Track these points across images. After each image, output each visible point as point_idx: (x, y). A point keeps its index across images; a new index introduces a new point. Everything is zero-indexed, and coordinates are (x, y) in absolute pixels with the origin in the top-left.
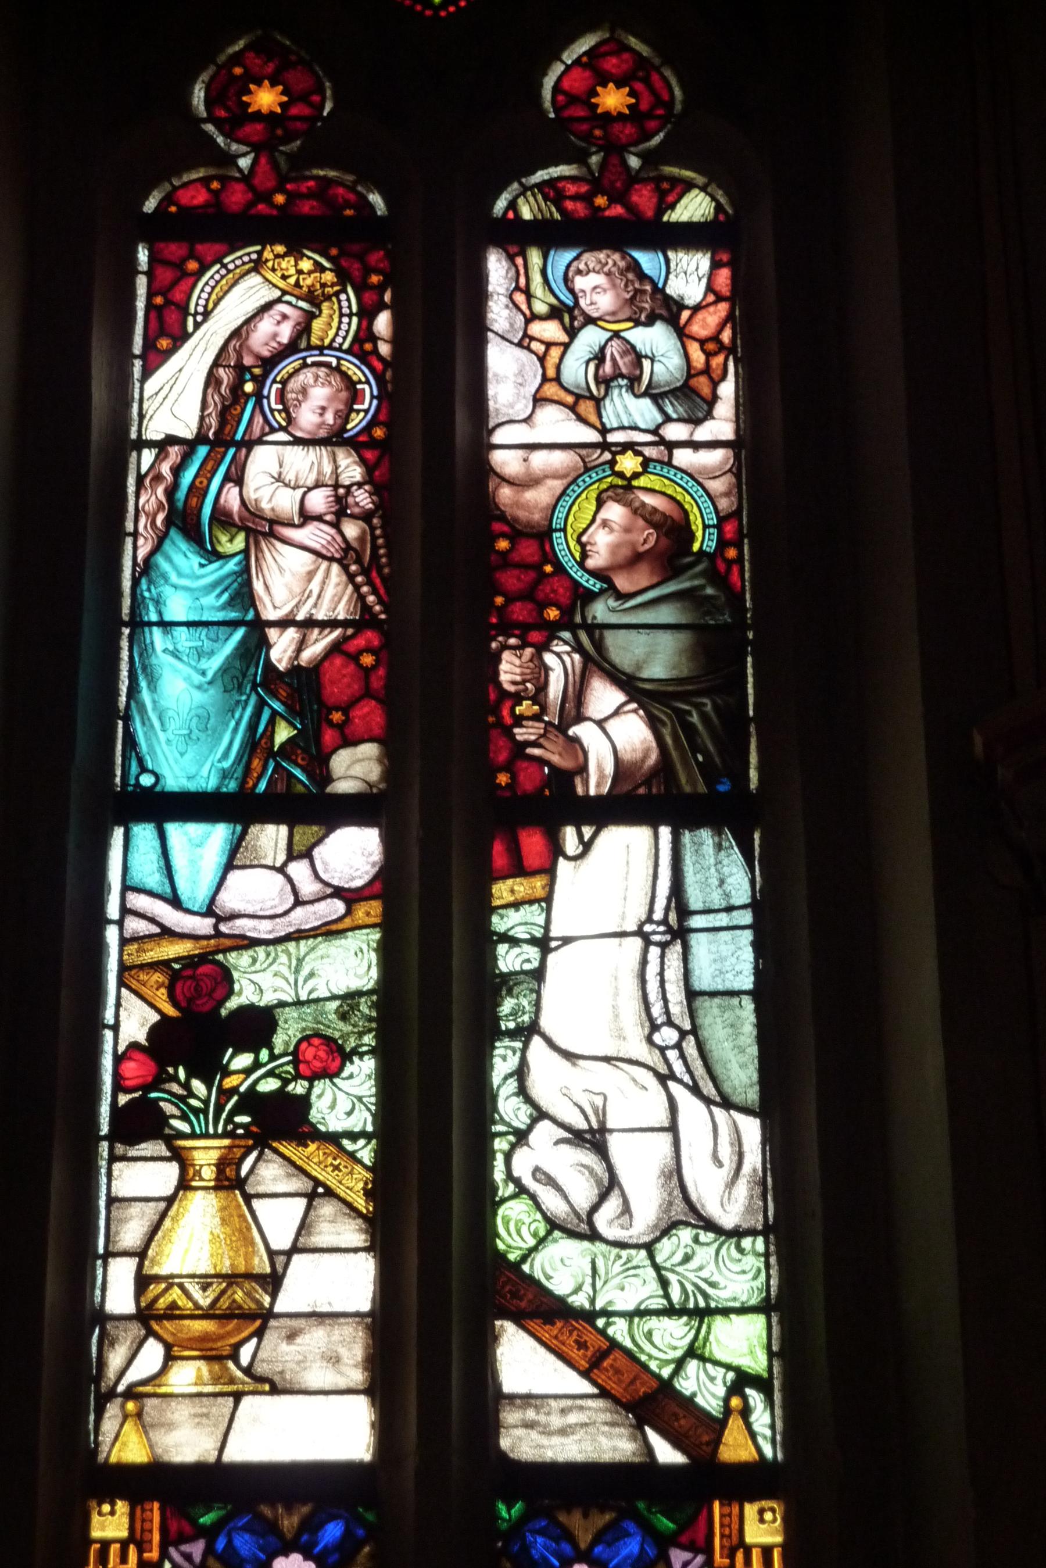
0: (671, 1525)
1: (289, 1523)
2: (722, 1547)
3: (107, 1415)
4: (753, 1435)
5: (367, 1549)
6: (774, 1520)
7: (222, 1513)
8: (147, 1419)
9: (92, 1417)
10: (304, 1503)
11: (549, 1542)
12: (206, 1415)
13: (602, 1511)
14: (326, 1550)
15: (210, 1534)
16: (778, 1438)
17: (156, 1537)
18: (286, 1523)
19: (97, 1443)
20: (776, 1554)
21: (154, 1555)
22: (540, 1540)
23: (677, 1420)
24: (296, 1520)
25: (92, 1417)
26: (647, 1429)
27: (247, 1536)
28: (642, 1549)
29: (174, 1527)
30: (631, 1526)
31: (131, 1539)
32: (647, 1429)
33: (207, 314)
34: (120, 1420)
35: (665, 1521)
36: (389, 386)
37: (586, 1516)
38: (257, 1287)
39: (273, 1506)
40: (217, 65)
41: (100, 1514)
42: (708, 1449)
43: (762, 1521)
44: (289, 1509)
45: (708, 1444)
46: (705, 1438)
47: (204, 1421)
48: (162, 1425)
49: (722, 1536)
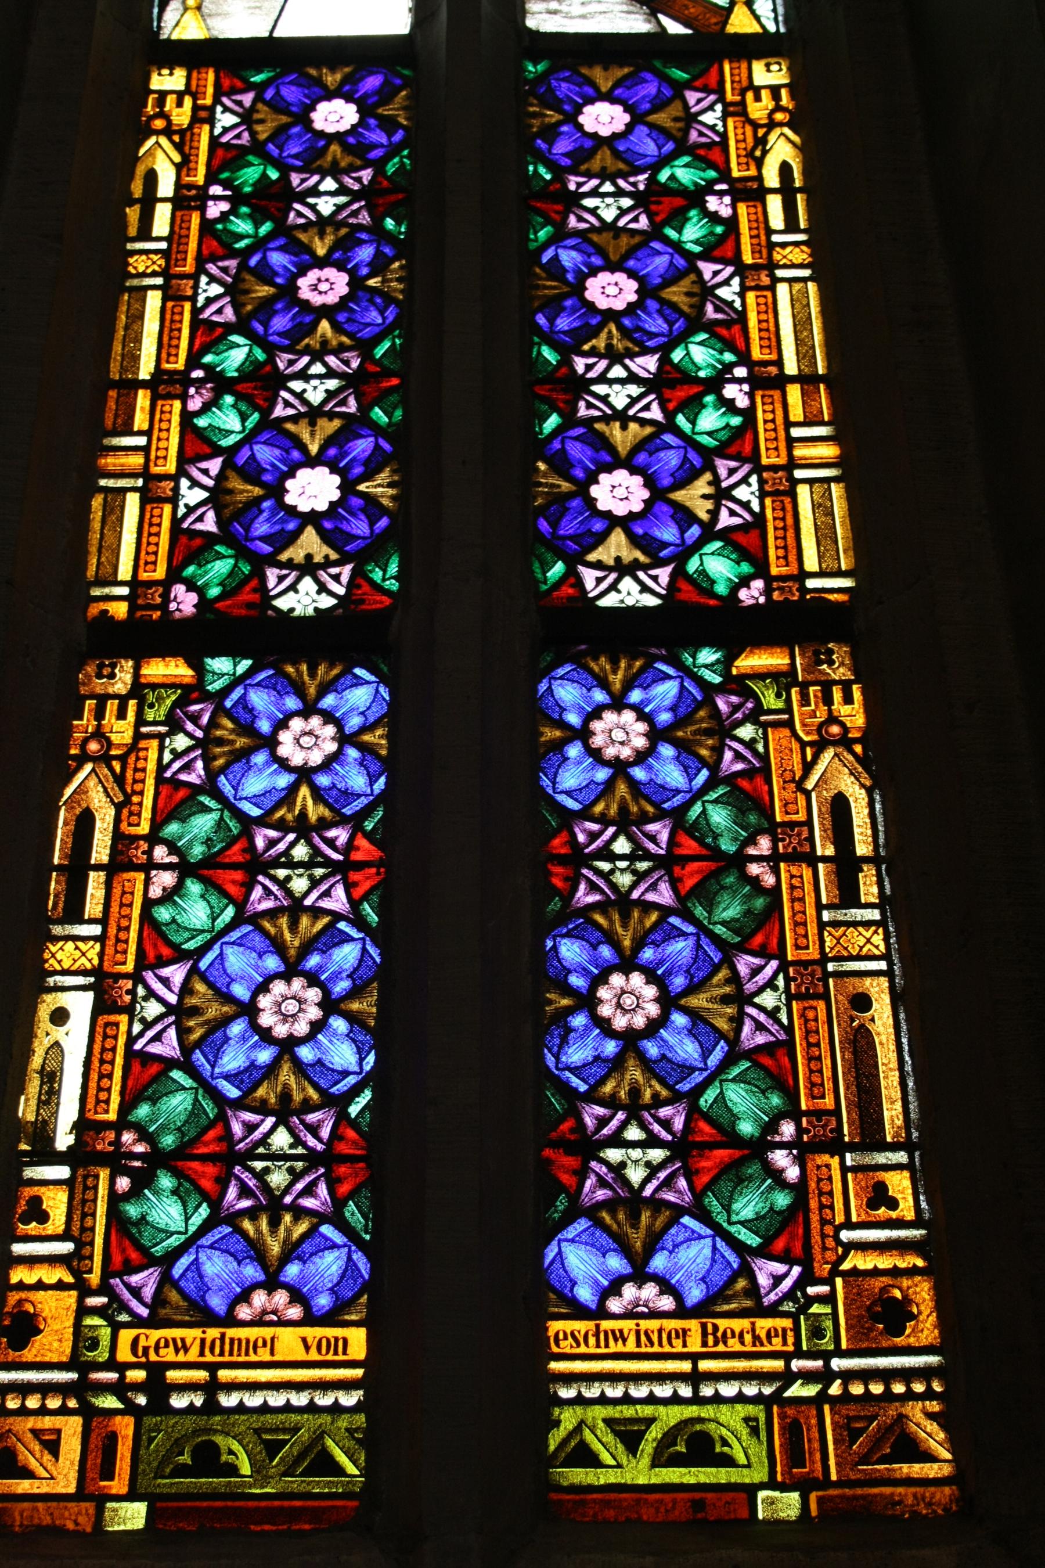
0: (685, 76)
1: (332, 79)
2: (733, 89)
3: (169, 8)
4: (757, 18)
5: (404, 93)
6: (780, 70)
7: (271, 74)
8: (205, 10)
9: (156, 11)
10: (347, 66)
11: (572, 87)
12: (259, 8)
13: (621, 66)
14: (366, 95)
15: (260, 89)
16: (780, 18)
17: (210, 90)
18: (330, 79)
19: (159, 27)
20: (784, 92)
21: (208, 101)
22: (564, 85)
23: (687, 8)
24: (338, 77)
25: (156, 11)
26: (660, 16)
27: (294, 88)
28: (659, 90)
29: (226, 83)
30: (649, 76)
31: (188, 90)
32: (660, 16)
33: (62, 1069)
34: (181, 11)
35: (679, 73)
36: (220, 226)
37: (606, 69)
38: (68, 792)
39: (318, 68)
40: (23, 1404)
41: (160, 74)
42: (717, 28)
43: (769, 71)
44: (333, 70)
45: (716, 24)
46: (714, 20)
47: (257, 11)
48: (219, 15)
49: (733, 82)
